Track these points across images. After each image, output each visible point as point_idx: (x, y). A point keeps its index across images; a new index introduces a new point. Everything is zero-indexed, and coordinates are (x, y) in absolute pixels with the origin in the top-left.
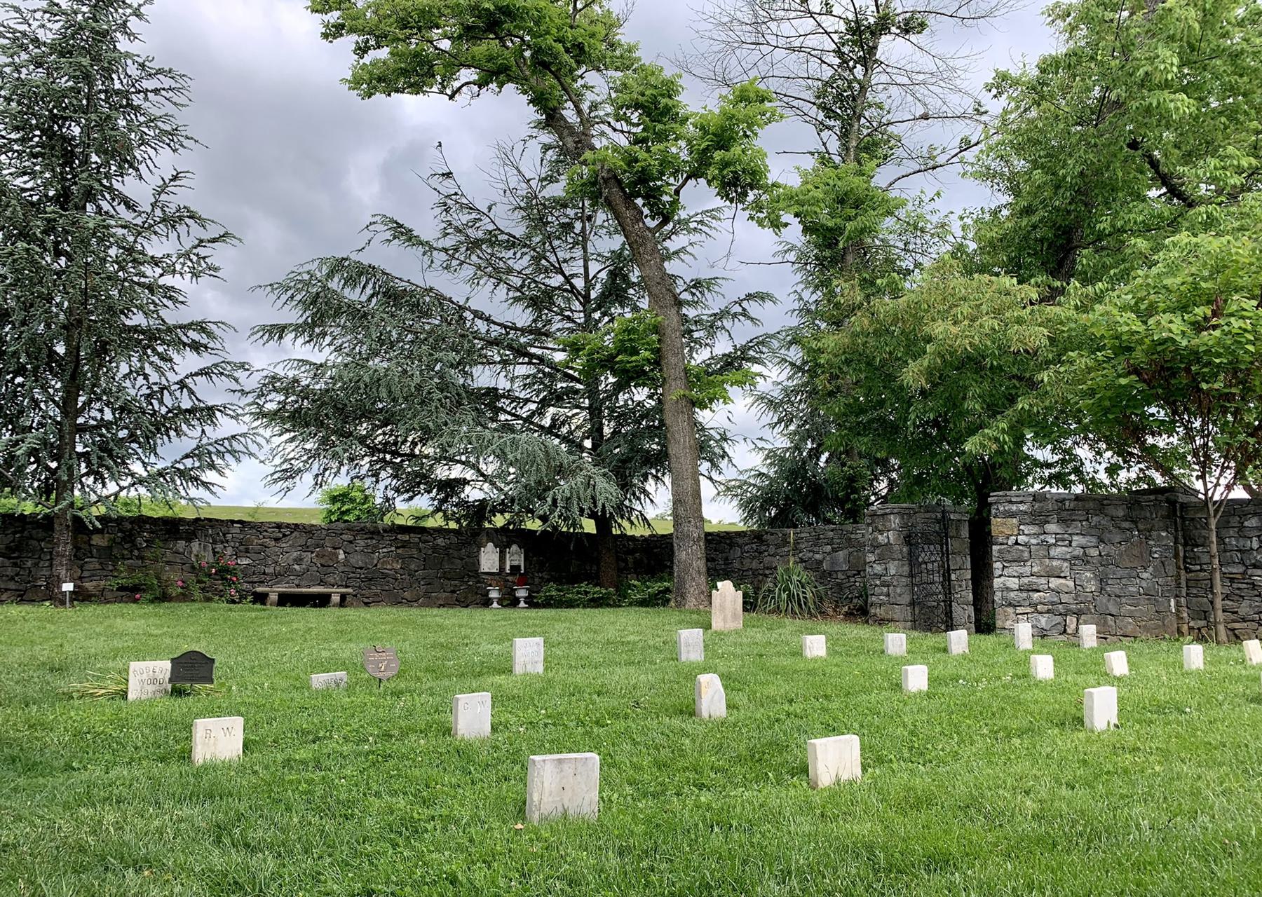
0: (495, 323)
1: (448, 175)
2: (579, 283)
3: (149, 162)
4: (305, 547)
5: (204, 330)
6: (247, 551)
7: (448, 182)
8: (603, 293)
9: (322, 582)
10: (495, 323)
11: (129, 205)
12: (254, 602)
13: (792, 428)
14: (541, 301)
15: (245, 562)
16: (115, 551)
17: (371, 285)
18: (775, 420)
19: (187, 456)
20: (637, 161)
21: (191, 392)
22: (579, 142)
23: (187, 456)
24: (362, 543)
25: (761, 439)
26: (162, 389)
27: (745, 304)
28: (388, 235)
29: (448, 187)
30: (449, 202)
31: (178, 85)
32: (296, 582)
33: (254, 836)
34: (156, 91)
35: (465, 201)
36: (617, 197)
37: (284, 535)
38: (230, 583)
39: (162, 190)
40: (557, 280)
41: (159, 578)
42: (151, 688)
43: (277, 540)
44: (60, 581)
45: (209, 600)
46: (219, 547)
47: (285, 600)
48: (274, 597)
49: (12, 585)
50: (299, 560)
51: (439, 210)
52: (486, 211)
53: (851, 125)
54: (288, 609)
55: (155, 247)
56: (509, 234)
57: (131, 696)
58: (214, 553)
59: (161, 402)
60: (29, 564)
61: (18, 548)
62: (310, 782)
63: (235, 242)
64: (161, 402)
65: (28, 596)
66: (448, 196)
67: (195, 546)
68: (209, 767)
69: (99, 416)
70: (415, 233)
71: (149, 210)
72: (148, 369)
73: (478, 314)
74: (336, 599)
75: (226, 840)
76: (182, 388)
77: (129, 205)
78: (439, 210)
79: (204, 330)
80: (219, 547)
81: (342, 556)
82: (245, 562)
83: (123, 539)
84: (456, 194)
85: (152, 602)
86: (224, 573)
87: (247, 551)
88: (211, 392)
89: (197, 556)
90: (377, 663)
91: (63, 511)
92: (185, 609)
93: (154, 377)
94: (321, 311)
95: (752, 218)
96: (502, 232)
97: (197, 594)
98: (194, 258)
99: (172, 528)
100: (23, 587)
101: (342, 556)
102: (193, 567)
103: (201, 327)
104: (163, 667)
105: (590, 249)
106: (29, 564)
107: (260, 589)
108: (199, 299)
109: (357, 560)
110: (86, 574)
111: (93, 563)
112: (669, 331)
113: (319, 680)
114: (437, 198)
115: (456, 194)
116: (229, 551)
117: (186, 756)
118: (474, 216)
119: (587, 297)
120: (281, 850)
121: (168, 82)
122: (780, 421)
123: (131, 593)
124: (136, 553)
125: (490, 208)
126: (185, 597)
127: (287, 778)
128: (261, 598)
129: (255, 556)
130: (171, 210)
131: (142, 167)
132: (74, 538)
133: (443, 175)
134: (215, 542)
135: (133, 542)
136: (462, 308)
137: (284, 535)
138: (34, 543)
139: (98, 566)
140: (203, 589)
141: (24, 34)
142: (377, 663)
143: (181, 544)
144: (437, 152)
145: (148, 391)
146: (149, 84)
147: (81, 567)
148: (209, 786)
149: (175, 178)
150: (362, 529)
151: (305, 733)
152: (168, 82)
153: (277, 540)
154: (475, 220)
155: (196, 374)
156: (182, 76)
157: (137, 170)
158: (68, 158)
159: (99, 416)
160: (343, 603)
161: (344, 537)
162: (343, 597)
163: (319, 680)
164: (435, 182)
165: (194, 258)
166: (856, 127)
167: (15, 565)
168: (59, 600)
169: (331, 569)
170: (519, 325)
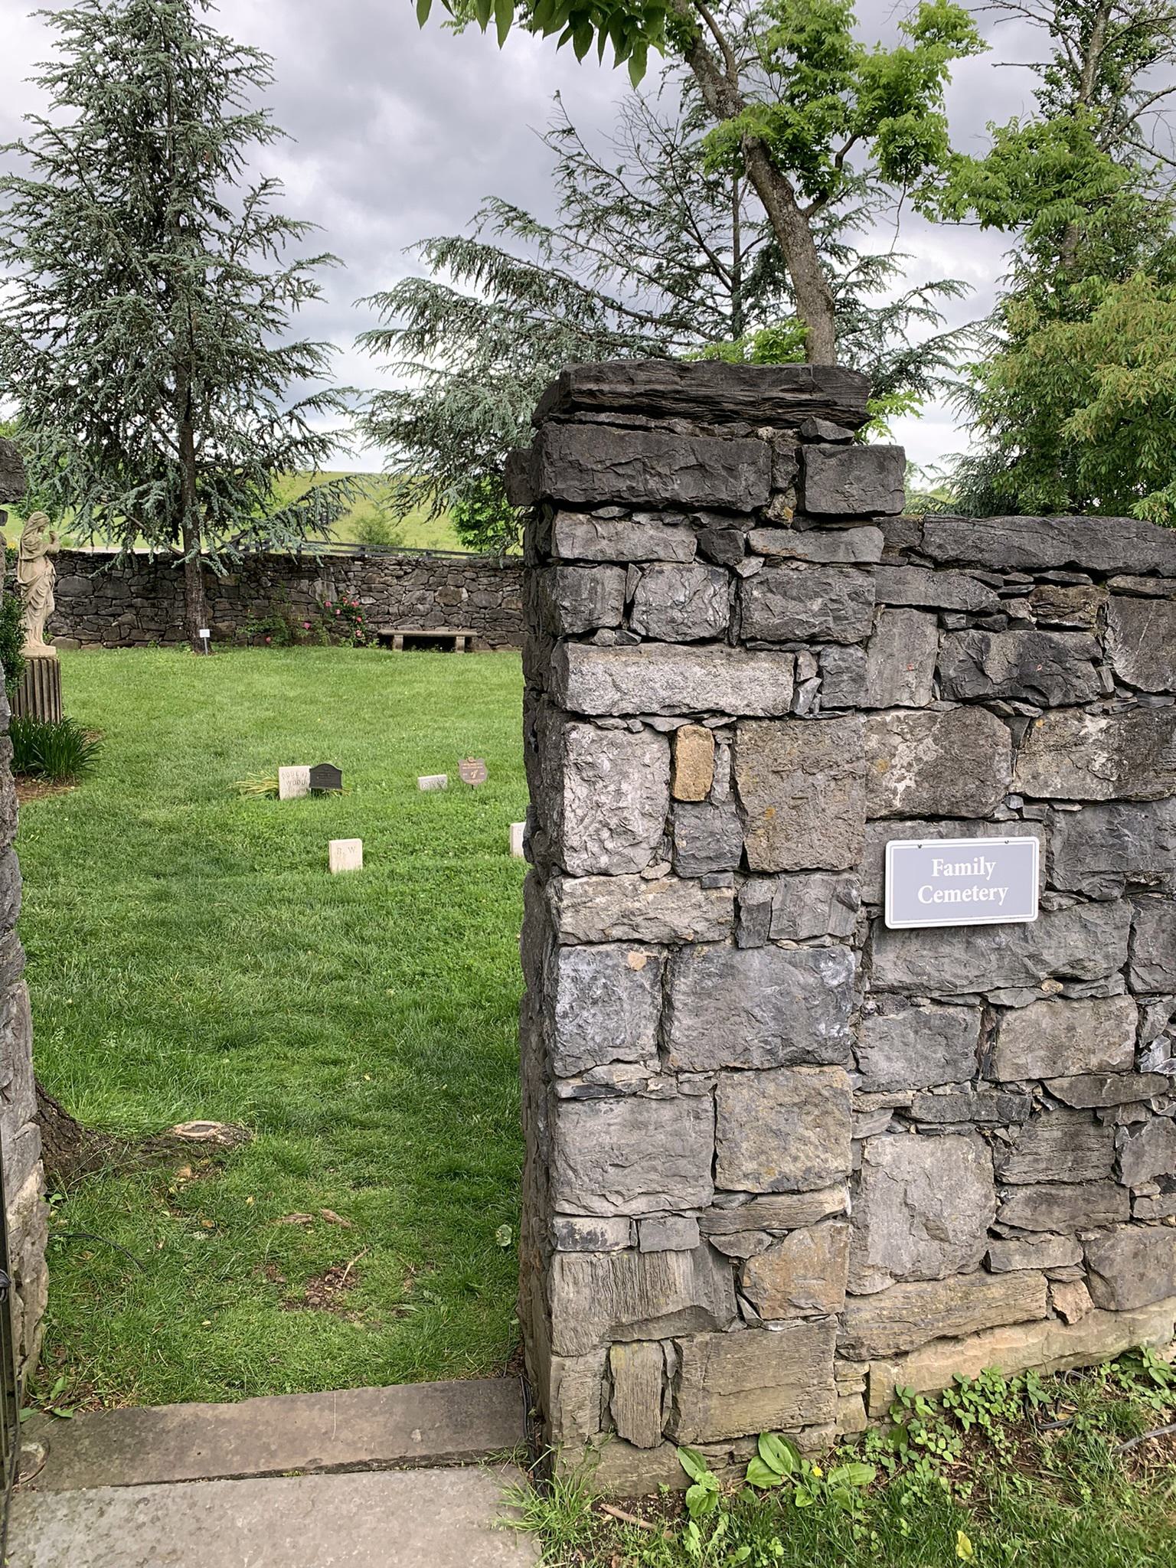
0: (628, 313)
1: (570, 131)
2: (727, 259)
3: (236, 158)
4: (427, 586)
5: (310, 352)
6: (370, 590)
7: (569, 141)
8: (753, 277)
9: (446, 623)
10: (628, 313)
11: (220, 212)
12: (380, 644)
13: (995, 431)
14: (681, 286)
15: (369, 601)
16: (242, 590)
17: (487, 267)
18: (976, 418)
19: (303, 498)
20: (787, 125)
21: (300, 422)
22: (722, 92)
23: (303, 498)
24: (485, 581)
25: (931, 466)
26: (272, 422)
27: (927, 293)
28: (501, 221)
29: (569, 145)
30: (573, 165)
31: (259, 63)
32: (421, 622)
33: (367, 933)
34: (237, 72)
35: (589, 162)
36: (763, 170)
37: (406, 573)
38: (356, 624)
39: (252, 200)
40: (701, 259)
41: (286, 619)
42: (297, 788)
43: (398, 578)
44: (197, 628)
45: (335, 642)
46: (342, 586)
47: (410, 643)
48: (399, 640)
49: (153, 626)
50: (422, 600)
51: (562, 175)
52: (615, 174)
53: (1095, 24)
54: (413, 653)
55: (254, 261)
56: (643, 203)
57: (282, 795)
58: (338, 592)
59: (271, 435)
60: (165, 604)
61: (154, 589)
62: (402, 894)
63: (334, 262)
64: (271, 435)
65: (169, 635)
66: (570, 158)
67: (319, 585)
68: (342, 877)
69: (212, 452)
70: (531, 217)
71: (242, 223)
72: (257, 404)
73: (608, 303)
74: (460, 642)
75: (352, 935)
76: (291, 421)
77: (220, 212)
78: (562, 175)
79: (310, 352)
80: (342, 586)
81: (465, 595)
82: (369, 601)
83: (249, 578)
84: (579, 154)
85: (282, 644)
86: (348, 613)
87: (370, 590)
88: (319, 423)
89: (321, 595)
90: (469, 771)
91: (193, 560)
92: (314, 652)
93: (263, 412)
94: (431, 314)
95: (918, 208)
96: (637, 201)
97: (326, 637)
98: (295, 283)
99: (295, 567)
100: (163, 627)
101: (465, 595)
102: (318, 607)
103: (305, 348)
104: (303, 772)
105: (742, 218)
106: (165, 604)
107: (385, 631)
108: (300, 321)
109: (481, 599)
110: (218, 614)
111: (223, 604)
112: (818, 345)
113: (426, 781)
114: (557, 160)
115: (579, 154)
116: (352, 590)
117: (325, 864)
118: (602, 180)
119: (736, 279)
120: (382, 943)
121: (248, 61)
122: (982, 421)
123: (262, 639)
124: (262, 592)
125: (620, 172)
126: (314, 640)
127: (390, 890)
128: (386, 641)
129: (378, 595)
130: (264, 221)
131: (230, 166)
132: (204, 579)
133: (564, 132)
134: (337, 581)
135: (258, 581)
136: (589, 294)
137: (406, 573)
138: (168, 583)
139: (228, 606)
140: (330, 630)
141: (95, 18)
142: (469, 771)
143: (305, 583)
144: (556, 103)
145: (258, 426)
146: (228, 65)
147: (213, 607)
148: (339, 894)
149: (264, 186)
150: (484, 566)
151: (406, 846)
152: (248, 61)
153: (398, 578)
154: (603, 186)
155: (304, 404)
156: (262, 55)
157: (225, 169)
158: (156, 158)
159: (212, 452)
160: (468, 646)
161: (467, 574)
162: (468, 640)
163: (426, 781)
164: (554, 140)
165: (295, 283)
166: (1102, 26)
167: (153, 605)
168: (199, 646)
169: (455, 609)
170: (656, 316)
